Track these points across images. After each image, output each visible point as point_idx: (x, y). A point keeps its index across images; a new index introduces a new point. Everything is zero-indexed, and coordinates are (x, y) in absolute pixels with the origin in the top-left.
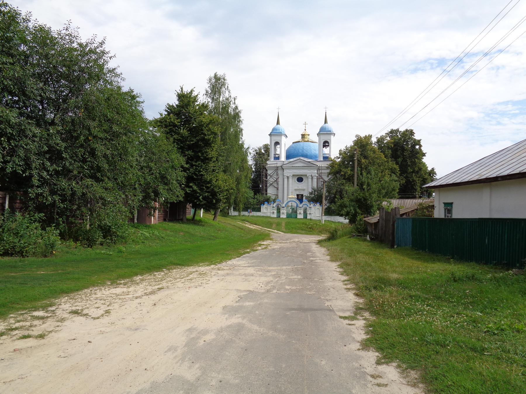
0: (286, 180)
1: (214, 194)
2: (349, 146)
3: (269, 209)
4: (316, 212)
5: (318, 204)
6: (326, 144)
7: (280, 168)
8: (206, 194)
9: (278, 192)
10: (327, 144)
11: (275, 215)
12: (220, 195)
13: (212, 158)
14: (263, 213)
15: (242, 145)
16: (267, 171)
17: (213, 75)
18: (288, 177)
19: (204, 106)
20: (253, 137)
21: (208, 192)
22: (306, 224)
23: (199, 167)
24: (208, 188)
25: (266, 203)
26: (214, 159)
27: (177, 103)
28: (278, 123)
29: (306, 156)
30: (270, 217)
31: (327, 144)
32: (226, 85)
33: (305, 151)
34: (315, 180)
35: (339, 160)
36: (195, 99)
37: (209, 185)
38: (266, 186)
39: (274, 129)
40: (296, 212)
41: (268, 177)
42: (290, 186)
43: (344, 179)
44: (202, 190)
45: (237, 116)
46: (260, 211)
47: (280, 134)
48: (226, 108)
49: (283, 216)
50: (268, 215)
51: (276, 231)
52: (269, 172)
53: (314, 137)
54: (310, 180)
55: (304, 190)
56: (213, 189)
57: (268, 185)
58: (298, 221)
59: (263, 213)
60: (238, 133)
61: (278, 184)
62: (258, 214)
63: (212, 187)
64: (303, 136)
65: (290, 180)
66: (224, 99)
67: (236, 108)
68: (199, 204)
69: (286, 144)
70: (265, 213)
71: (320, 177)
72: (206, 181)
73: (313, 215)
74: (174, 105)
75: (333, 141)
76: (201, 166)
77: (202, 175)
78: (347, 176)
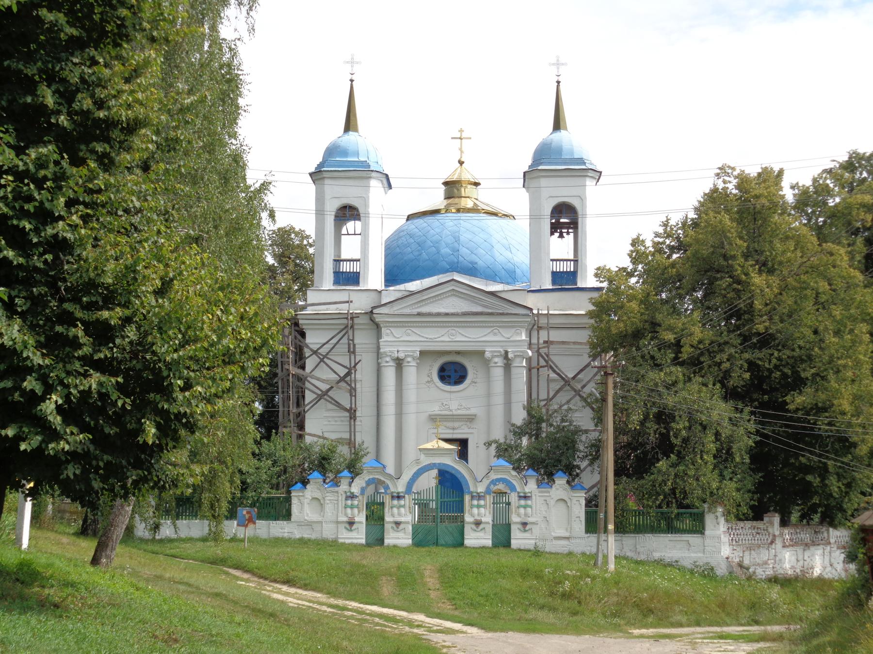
0: (389, 375)
1: (147, 382)
2: (676, 219)
3: (329, 508)
4: (552, 518)
5: (561, 480)
6: (565, 218)
7: (364, 320)
8: (94, 380)
9: (352, 431)
11: (359, 536)
12: (188, 386)
13: (132, 127)
14: (300, 524)
16: (303, 335)
18: (399, 363)
21: (102, 366)
22: (538, 576)
23: (40, 184)
24: (103, 333)
25: (315, 477)
26: (145, 142)
28: (350, 124)
29: (472, 271)
30: (334, 544)
33: (464, 251)
34: (520, 376)
37: (112, 316)
39: (332, 151)
40: (382, 519)
41: (310, 364)
42: (411, 395)
43: (676, 361)
44: (56, 345)
46: (287, 516)
47: (362, 172)
49: (399, 538)
50: (328, 532)
52: (313, 339)
53: (505, 192)
54: (498, 373)
55: (470, 419)
56: (142, 346)
57: (309, 397)
58: (520, 562)
59: (300, 524)
61: (353, 392)
62: (278, 529)
63: (131, 333)
64: (452, 187)
65: (411, 373)
68: (39, 452)
69: (386, 214)
70: (310, 524)
71: (541, 362)
72: (92, 285)
73: (536, 530)
75: (594, 201)
76: (60, 177)
77: (60, 245)
78: (687, 352)
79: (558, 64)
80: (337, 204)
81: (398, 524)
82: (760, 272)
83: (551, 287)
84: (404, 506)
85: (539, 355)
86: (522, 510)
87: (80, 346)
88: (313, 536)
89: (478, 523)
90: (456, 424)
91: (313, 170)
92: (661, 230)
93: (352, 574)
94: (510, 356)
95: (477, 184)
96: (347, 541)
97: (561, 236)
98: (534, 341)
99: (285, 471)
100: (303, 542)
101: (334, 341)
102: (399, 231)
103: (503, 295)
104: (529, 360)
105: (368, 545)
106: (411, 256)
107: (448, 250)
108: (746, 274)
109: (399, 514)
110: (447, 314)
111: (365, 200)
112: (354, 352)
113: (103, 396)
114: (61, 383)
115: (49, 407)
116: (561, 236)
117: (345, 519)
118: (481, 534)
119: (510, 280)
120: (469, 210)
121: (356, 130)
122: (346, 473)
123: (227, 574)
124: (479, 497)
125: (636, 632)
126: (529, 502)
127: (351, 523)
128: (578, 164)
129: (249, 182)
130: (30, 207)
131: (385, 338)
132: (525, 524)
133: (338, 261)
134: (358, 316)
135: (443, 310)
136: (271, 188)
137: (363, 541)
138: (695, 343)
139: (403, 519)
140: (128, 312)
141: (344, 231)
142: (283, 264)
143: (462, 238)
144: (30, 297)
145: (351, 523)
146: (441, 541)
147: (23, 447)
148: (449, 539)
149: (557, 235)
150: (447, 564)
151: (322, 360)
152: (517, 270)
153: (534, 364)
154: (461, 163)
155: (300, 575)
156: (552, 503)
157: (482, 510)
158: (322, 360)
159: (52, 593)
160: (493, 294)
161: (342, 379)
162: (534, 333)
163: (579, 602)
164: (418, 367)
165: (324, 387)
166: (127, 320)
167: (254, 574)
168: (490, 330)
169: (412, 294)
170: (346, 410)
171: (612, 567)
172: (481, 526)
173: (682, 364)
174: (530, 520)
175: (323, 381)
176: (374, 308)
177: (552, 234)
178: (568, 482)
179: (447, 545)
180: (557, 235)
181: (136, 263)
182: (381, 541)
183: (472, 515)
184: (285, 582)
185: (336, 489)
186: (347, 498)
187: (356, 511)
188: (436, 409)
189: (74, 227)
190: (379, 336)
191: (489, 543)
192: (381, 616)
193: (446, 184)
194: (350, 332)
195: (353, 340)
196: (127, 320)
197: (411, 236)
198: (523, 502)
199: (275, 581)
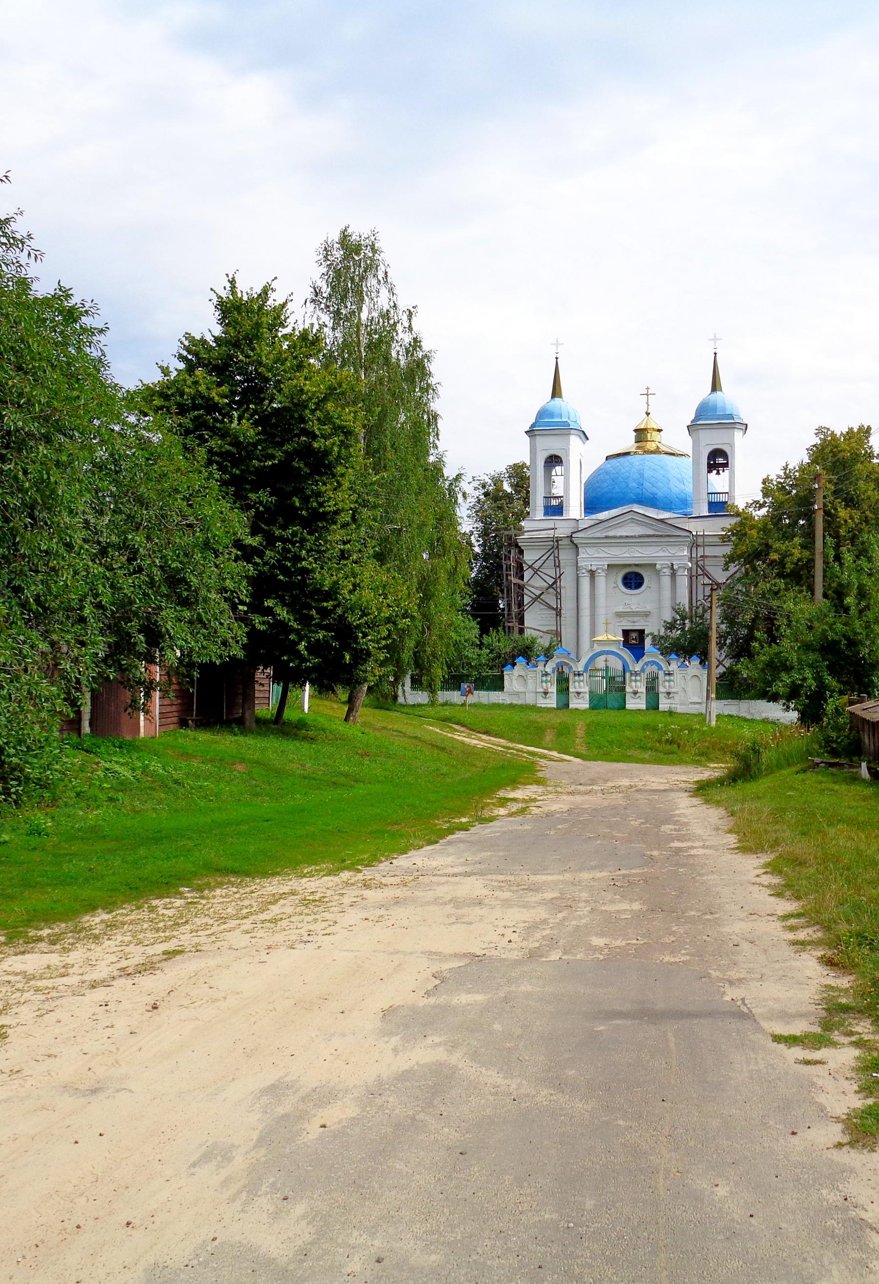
0: (585, 582)
2: (794, 464)
3: (530, 682)
5: (696, 661)
6: (718, 460)
8: (321, 635)
9: (558, 624)
10: (721, 460)
11: (551, 702)
15: (437, 470)
16: (521, 552)
17: (336, 237)
18: (592, 574)
19: (308, 341)
20: (474, 440)
21: (327, 628)
22: (655, 729)
23: (293, 544)
24: (324, 613)
27: (218, 330)
28: (556, 392)
29: (652, 502)
30: (534, 708)
31: (721, 460)
32: (382, 268)
33: (647, 485)
34: (683, 581)
35: (764, 511)
36: (278, 317)
37: (329, 605)
38: (520, 604)
39: (542, 414)
41: (527, 575)
43: (780, 575)
44: (304, 620)
45: (417, 370)
46: (501, 688)
47: (564, 429)
48: (380, 344)
49: (579, 703)
50: (530, 700)
51: (555, 754)
52: (529, 557)
54: (666, 581)
55: (647, 614)
56: (342, 618)
57: (527, 600)
60: (423, 427)
61: (558, 596)
62: (495, 697)
63: (339, 611)
64: (641, 434)
65: (601, 581)
66: (375, 314)
67: (416, 343)
68: (298, 667)
70: (517, 694)
71: (698, 571)
74: (209, 338)
75: (741, 448)
76: (303, 541)
77: (305, 571)
78: (789, 567)
79: (557, 344)
80: (546, 454)
81: (578, 693)
82: (847, 506)
83: (707, 514)
84: (583, 681)
85: (698, 566)
86: (667, 684)
87: (315, 619)
88: (519, 702)
89: (635, 693)
90: (635, 619)
91: (528, 429)
92: (782, 473)
93: (528, 728)
94: (675, 567)
95: (660, 431)
96: (543, 706)
97: (718, 473)
98: (694, 555)
99: (499, 656)
100: (512, 706)
101: (544, 558)
102: (599, 469)
103: (670, 522)
104: (690, 570)
105: (558, 708)
106: (606, 490)
107: (635, 485)
108: (836, 509)
109: (580, 687)
110: (627, 537)
111: (567, 451)
112: (559, 566)
113: (327, 642)
114: (306, 636)
115: (302, 646)
116: (718, 473)
117: (542, 690)
118: (638, 701)
119: (682, 506)
120: (652, 452)
121: (561, 397)
122: (542, 658)
123: (451, 727)
124: (636, 674)
125: (712, 765)
126: (672, 678)
127: (546, 693)
128: (728, 419)
129: (446, 475)
130: (289, 555)
131: (581, 555)
132: (669, 693)
133: (547, 498)
134: (561, 539)
135: (624, 534)
136: (463, 477)
137: (555, 706)
138: (795, 561)
139: (582, 690)
140: (335, 603)
141: (553, 473)
142: (518, 492)
143: (646, 475)
144: (291, 596)
145: (546, 693)
146: (610, 706)
147: (291, 665)
148: (616, 705)
149: (715, 472)
150: (593, 722)
151: (536, 573)
152: (689, 499)
153: (694, 573)
154: (648, 414)
155: (494, 728)
156: (688, 678)
157: (638, 683)
158: (536, 573)
159: (311, 733)
160: (662, 521)
161: (551, 586)
162: (694, 549)
163: (679, 747)
164: (606, 576)
165: (538, 593)
166: (335, 607)
167: (468, 728)
168: (660, 548)
169: (602, 522)
170: (553, 609)
171: (713, 723)
172: (638, 695)
173: (784, 577)
174: (673, 690)
175: (536, 588)
176: (573, 533)
177: (710, 471)
178: (700, 663)
179: (613, 709)
180: (715, 472)
181: (338, 581)
182: (567, 705)
183: (632, 687)
184: (485, 733)
185: (535, 669)
186: (543, 675)
187: (549, 684)
188: (621, 609)
189: (311, 563)
190: (577, 555)
191: (644, 707)
192: (529, 753)
193: (636, 431)
194: (556, 551)
195: (558, 557)
196: (338, 605)
197: (607, 473)
198: (667, 678)
199: (479, 732)
